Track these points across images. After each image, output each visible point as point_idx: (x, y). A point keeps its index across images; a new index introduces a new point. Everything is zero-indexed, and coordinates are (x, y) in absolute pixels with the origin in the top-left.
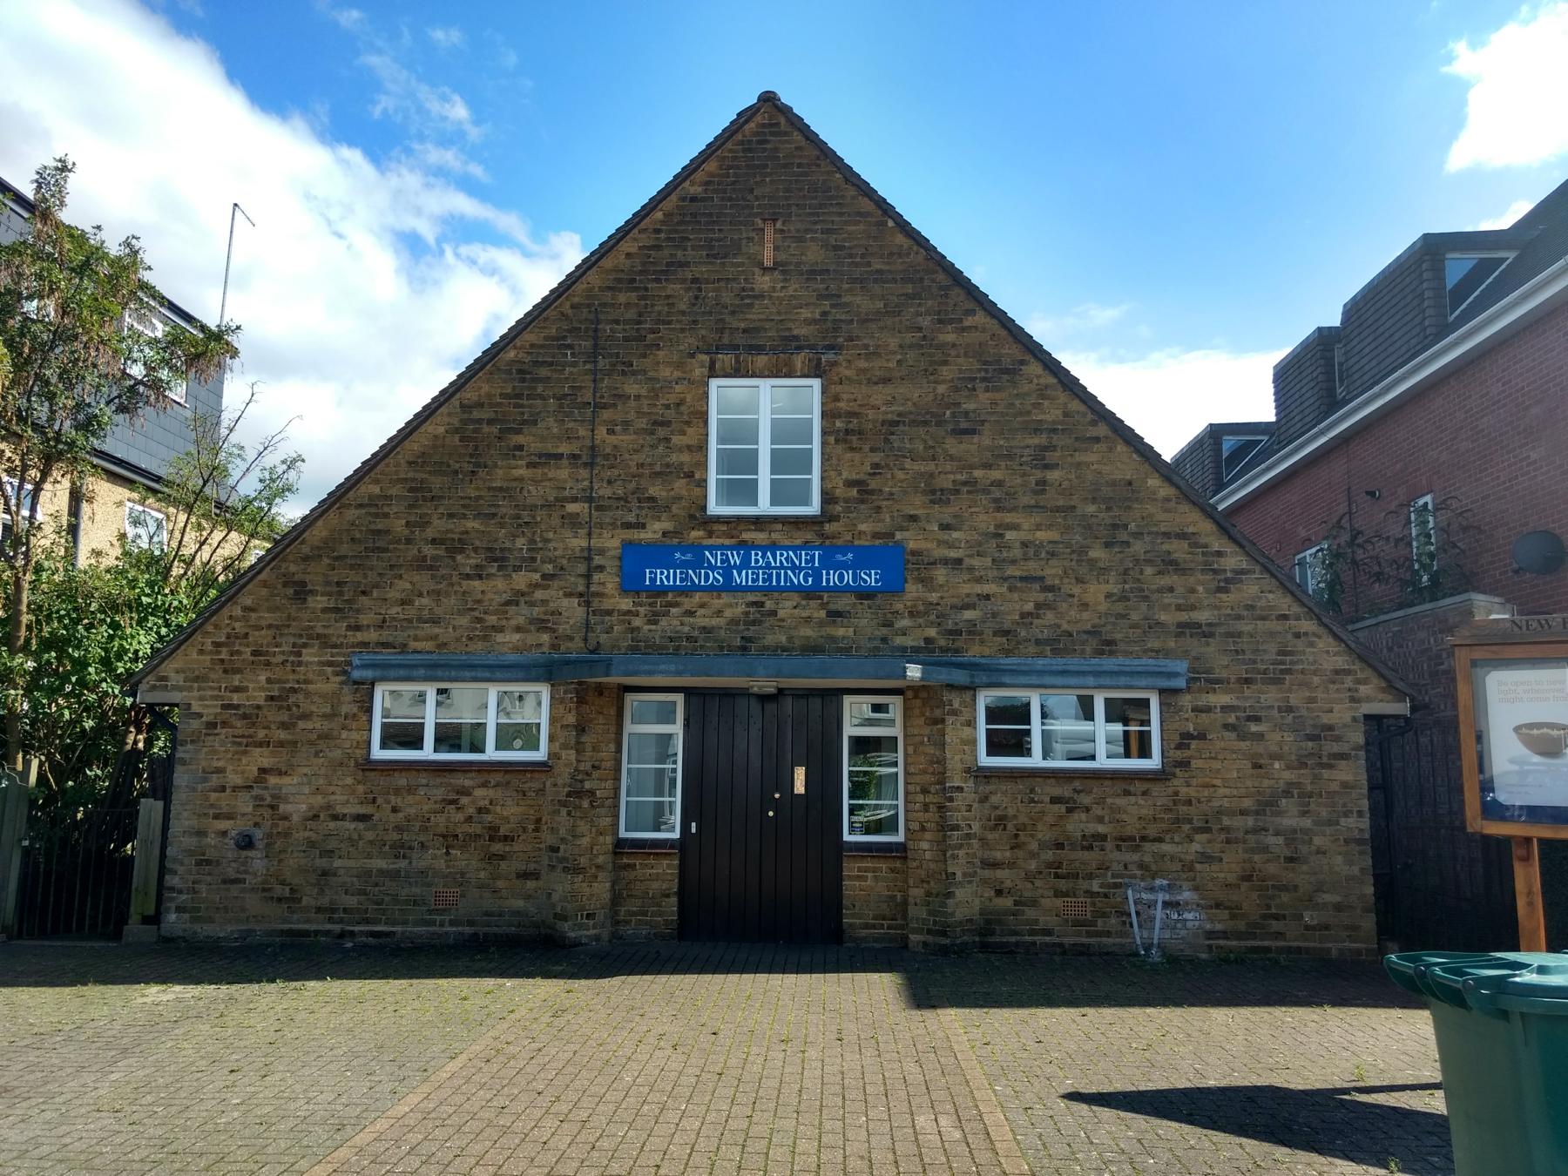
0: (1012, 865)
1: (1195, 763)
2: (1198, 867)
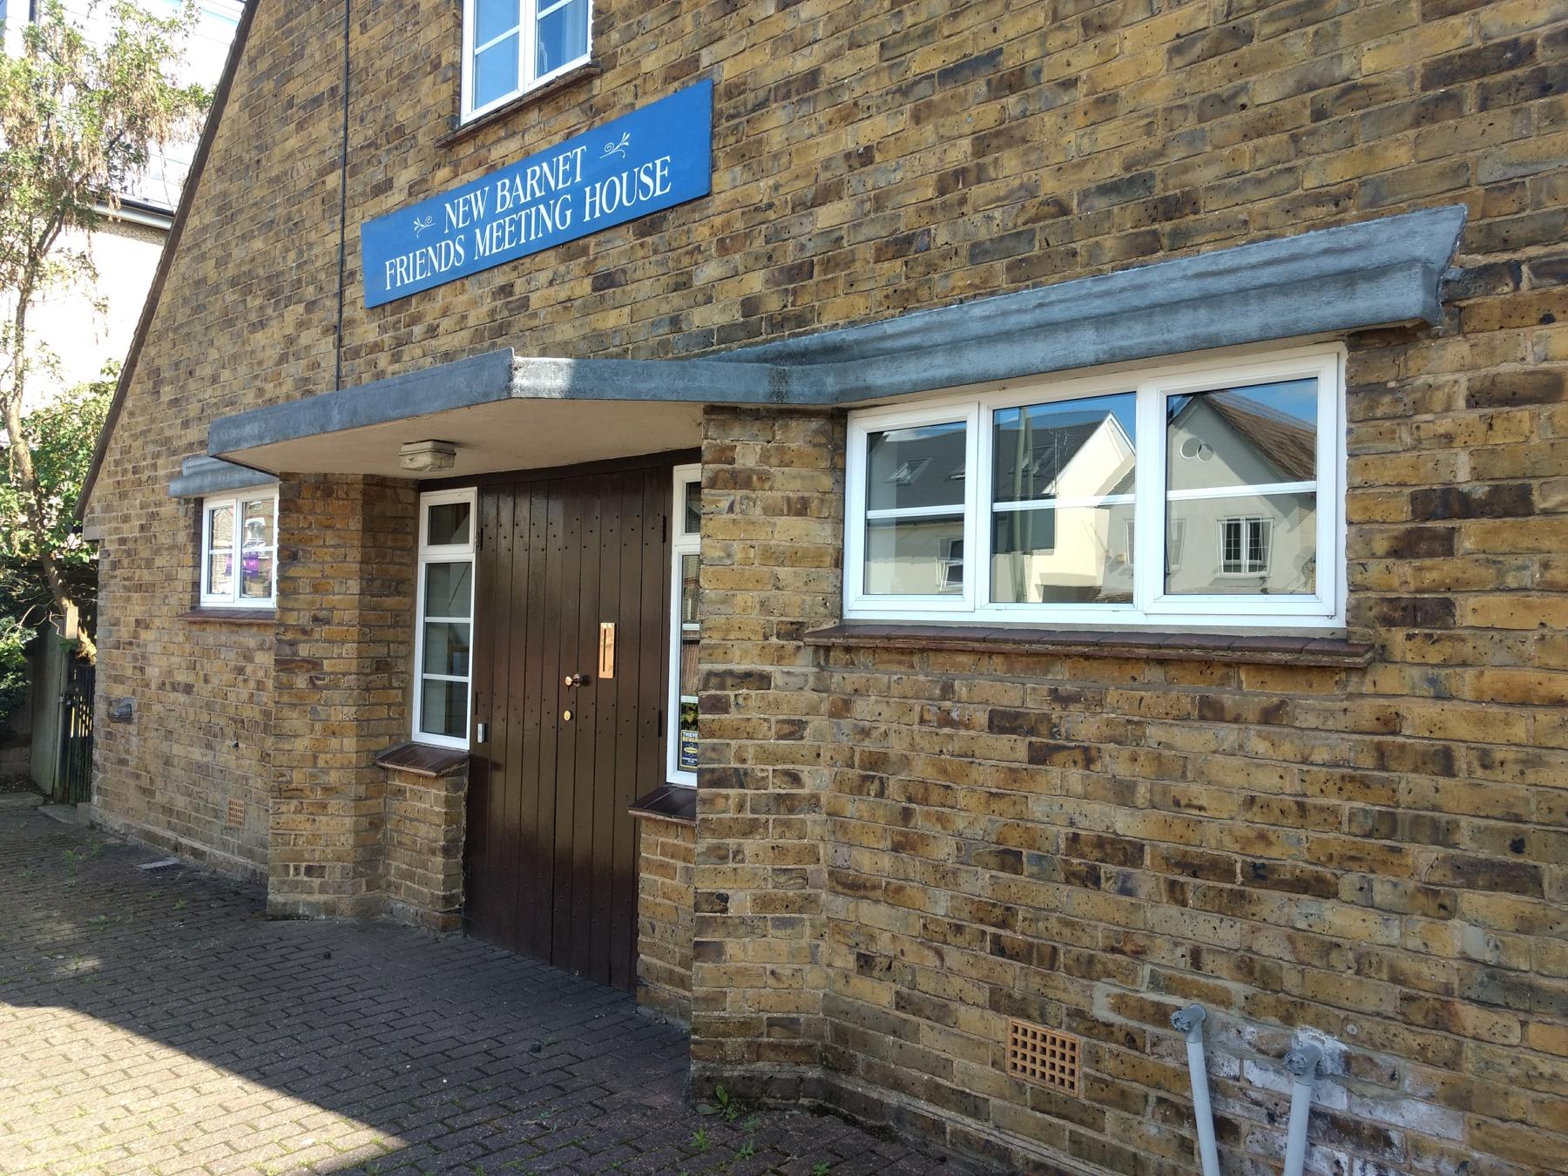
0: (894, 894)
1: (1469, 611)
2: (1471, 1016)
